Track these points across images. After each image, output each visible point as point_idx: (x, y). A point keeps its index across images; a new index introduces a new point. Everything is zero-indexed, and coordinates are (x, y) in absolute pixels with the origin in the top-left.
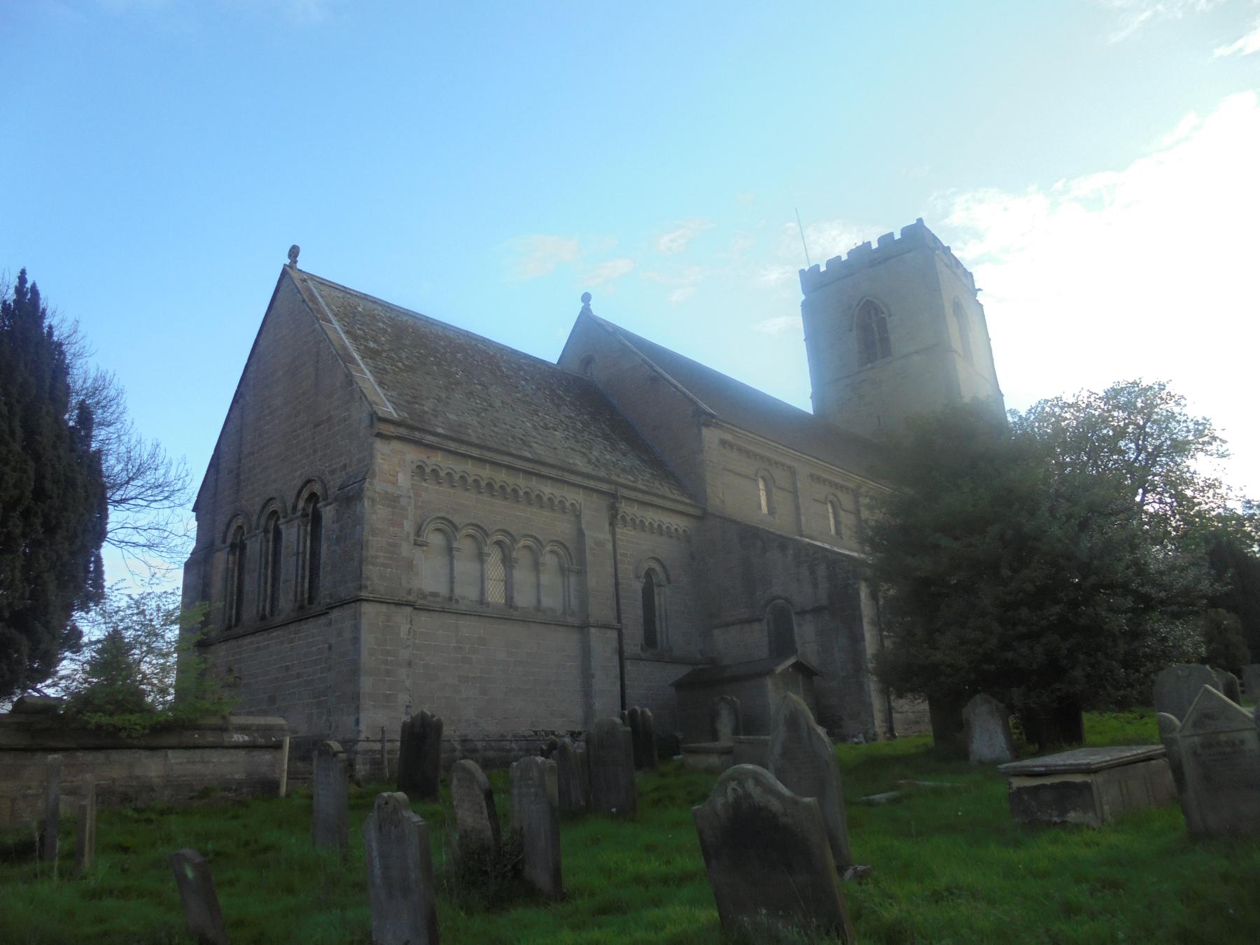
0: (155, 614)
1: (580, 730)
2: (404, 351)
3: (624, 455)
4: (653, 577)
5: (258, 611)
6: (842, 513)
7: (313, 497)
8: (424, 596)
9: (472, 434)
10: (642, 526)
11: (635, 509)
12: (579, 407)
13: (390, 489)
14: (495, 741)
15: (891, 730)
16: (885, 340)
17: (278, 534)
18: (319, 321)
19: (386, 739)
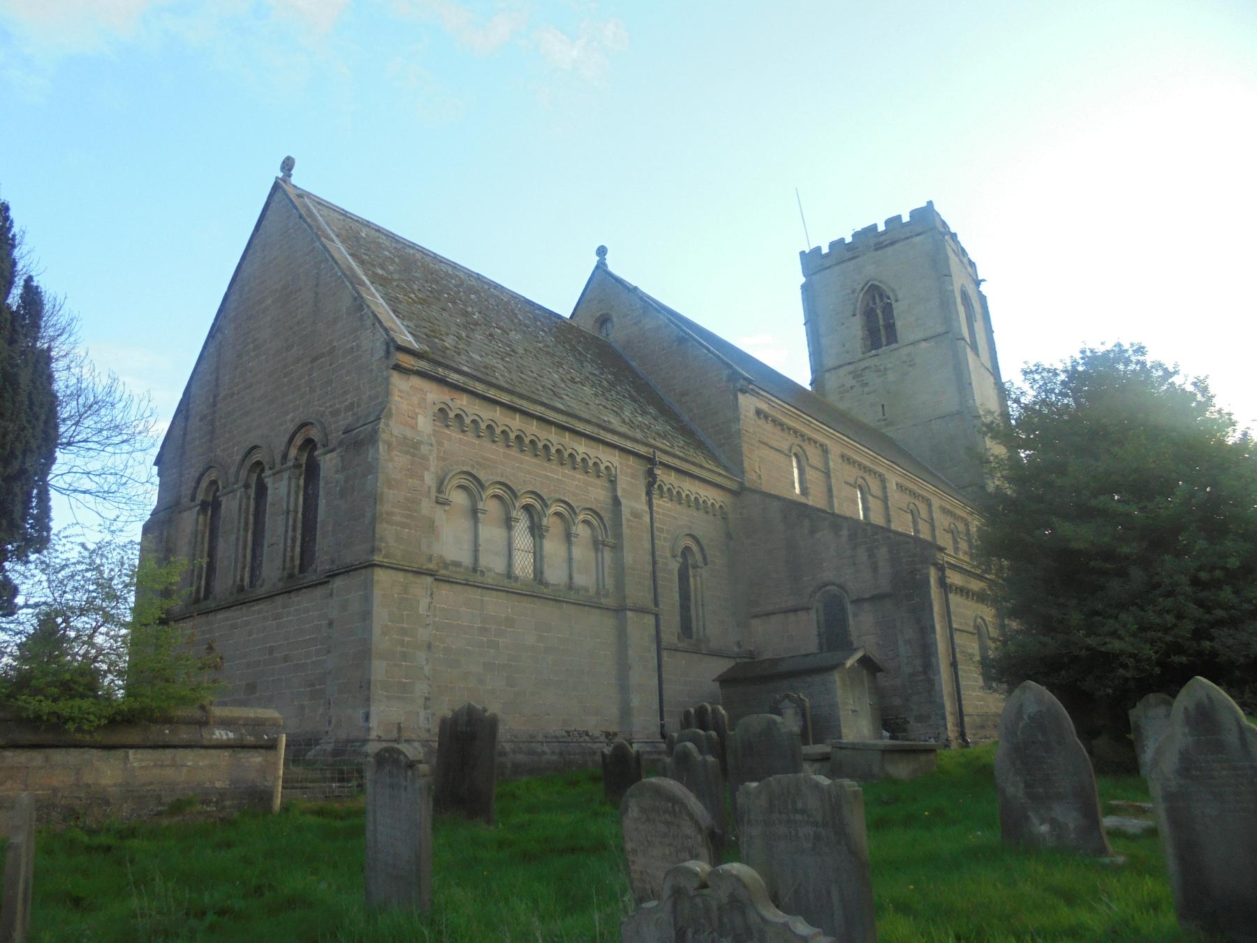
0: (117, 570)
1: (615, 730)
2: (415, 283)
3: (655, 419)
4: (689, 557)
5: (234, 581)
6: (870, 498)
7: (309, 444)
8: (446, 565)
9: (500, 378)
10: (678, 498)
11: (672, 478)
12: (601, 366)
13: (409, 433)
14: (524, 742)
15: (962, 735)
16: (891, 328)
17: (262, 490)
18: (320, 238)
19: (403, 738)
